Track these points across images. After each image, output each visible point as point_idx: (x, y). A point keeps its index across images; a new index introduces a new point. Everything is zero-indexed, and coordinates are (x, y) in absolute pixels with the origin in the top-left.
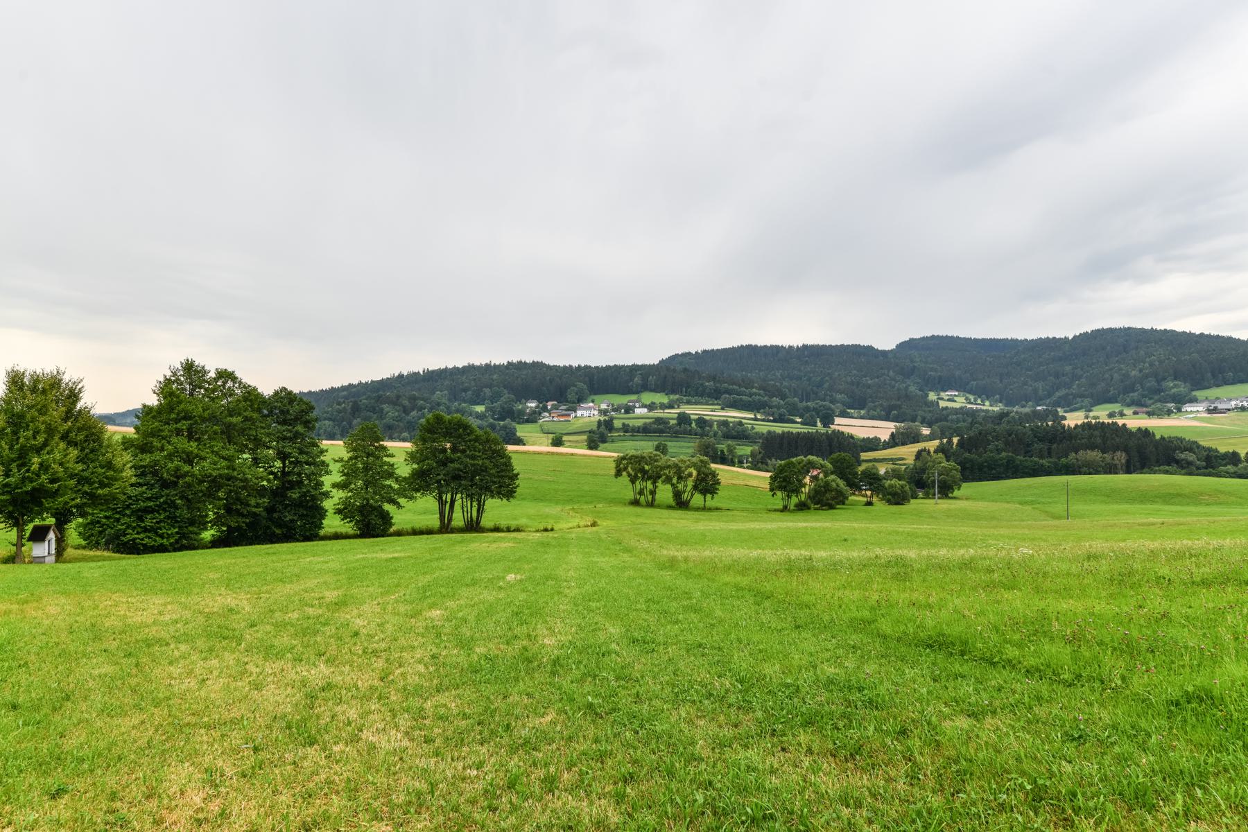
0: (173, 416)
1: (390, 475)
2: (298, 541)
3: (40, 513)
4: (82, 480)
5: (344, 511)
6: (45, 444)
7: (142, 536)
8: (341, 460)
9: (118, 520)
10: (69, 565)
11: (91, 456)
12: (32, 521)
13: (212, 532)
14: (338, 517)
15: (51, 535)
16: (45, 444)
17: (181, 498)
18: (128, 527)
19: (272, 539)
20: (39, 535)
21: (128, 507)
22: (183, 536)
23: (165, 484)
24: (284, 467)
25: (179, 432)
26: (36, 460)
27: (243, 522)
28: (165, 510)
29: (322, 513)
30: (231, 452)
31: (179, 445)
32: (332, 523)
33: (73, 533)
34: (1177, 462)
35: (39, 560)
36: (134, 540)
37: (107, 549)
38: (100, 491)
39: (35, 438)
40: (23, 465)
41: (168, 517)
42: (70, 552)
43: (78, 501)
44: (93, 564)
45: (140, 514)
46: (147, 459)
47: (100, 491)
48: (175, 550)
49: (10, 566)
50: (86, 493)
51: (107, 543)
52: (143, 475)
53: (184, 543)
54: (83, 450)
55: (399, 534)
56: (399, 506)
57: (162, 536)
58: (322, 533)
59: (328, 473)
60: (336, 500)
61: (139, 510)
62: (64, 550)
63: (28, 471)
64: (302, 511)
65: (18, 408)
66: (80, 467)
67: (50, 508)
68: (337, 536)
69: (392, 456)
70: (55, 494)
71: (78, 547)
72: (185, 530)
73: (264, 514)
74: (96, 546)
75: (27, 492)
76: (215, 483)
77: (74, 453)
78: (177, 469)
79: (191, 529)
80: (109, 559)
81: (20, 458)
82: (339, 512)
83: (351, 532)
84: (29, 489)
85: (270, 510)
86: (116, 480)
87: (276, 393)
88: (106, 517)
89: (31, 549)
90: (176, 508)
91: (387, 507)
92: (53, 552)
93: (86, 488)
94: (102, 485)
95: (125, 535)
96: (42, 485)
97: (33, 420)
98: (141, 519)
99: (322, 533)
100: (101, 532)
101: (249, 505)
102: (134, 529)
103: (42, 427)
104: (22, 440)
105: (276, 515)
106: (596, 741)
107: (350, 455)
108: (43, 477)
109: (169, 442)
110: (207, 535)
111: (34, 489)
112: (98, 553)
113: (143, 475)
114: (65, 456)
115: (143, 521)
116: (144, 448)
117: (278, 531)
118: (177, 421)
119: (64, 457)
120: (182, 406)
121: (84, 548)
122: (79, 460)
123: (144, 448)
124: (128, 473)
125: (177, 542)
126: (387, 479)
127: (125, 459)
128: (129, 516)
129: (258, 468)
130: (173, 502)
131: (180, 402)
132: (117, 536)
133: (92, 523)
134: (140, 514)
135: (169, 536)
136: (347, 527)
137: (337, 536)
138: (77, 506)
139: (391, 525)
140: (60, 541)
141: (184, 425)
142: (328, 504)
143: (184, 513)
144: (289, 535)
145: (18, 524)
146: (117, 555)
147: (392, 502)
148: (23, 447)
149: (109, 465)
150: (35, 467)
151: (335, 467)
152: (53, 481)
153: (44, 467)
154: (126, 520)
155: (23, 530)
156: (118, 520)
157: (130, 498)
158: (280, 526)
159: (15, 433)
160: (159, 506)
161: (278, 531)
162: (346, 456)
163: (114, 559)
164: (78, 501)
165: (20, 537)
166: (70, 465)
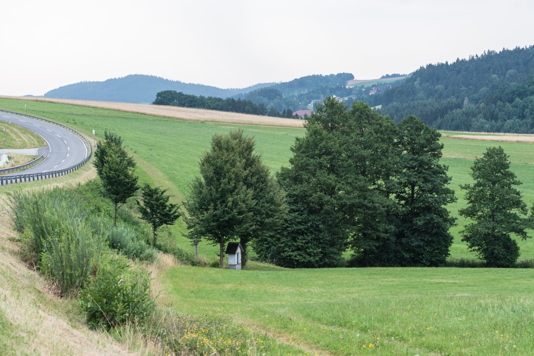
0: (317, 152)
1: (517, 203)
2: (424, 265)
3: (232, 235)
4: (257, 212)
5: (471, 238)
6: (235, 188)
7: (296, 253)
8: (467, 187)
9: (279, 239)
10: (251, 272)
11: (261, 194)
12: (228, 240)
13: (352, 252)
14: (465, 246)
15: (239, 250)
16: (235, 188)
17: (324, 223)
18: (286, 245)
19: (402, 263)
20: (231, 250)
21: (286, 228)
22: (325, 255)
23: (312, 211)
24: (413, 193)
25: (321, 166)
26: (230, 199)
27: (373, 245)
28: (311, 233)
29: (448, 240)
30: (361, 183)
31: (321, 178)
32: (459, 249)
33: (251, 252)
34: (422, 263)
35: (231, 267)
36: (290, 256)
37: (272, 262)
38: (267, 220)
39: (229, 183)
40: (223, 202)
41: (315, 239)
42: (249, 263)
43: (254, 227)
44: (264, 272)
45: (295, 235)
46: (298, 189)
47: (267, 220)
48: (320, 267)
49: (216, 269)
50: (258, 221)
51: (272, 258)
52: (295, 202)
53: (327, 261)
54: (255, 190)
55: (525, 265)
56: (524, 235)
57: (309, 254)
58: (448, 259)
59: (453, 200)
60: (461, 228)
61: (293, 232)
62: (246, 261)
63: (226, 206)
64: (427, 238)
65: (219, 162)
66: (254, 202)
67: (239, 232)
68: (463, 264)
69: (519, 183)
70: (240, 222)
71: (253, 259)
72: (327, 251)
73: (393, 239)
74: (264, 259)
75: (226, 221)
76: (351, 209)
77: (251, 192)
78: (320, 198)
79: (332, 250)
80: (273, 269)
81: (221, 197)
82: (466, 239)
83: (478, 261)
84: (227, 218)
85: (400, 235)
86: (276, 211)
87: (462, 60)
88: (271, 236)
89: (227, 259)
90: (320, 231)
91: (513, 236)
92: (240, 262)
93: (258, 218)
94: (268, 216)
95: (284, 252)
96: (233, 216)
97: (228, 171)
98: (294, 239)
99: (448, 259)
100: (268, 248)
101: (378, 231)
102: (290, 247)
103: (233, 176)
104: (222, 185)
105: (404, 240)
106: (330, 299)
107: (476, 182)
108: (235, 211)
109: (314, 175)
110: (348, 254)
111: (229, 219)
112: (267, 265)
113: (295, 202)
114: (246, 195)
115: (296, 241)
116: (297, 180)
117: (407, 256)
118: (320, 156)
119: (245, 195)
120: (324, 143)
121: (257, 260)
122: (255, 197)
123: (297, 180)
124: (284, 207)
125: (321, 259)
126: (511, 207)
127: (281, 195)
128: (286, 237)
129: (389, 195)
130: (317, 226)
131: (322, 140)
132: (280, 251)
133: (262, 241)
134: (295, 235)
135: (315, 255)
136: (474, 256)
137: (463, 264)
138: (254, 231)
139: (517, 255)
140: (244, 254)
141: (325, 160)
142: (452, 231)
143: (326, 236)
144: (416, 261)
145: (220, 241)
146: (279, 267)
147: (521, 232)
148: (223, 189)
149: (271, 201)
150: (230, 204)
151: (461, 195)
152: (240, 213)
153: (235, 204)
154: (283, 239)
155: (224, 246)
156: (279, 239)
157: (286, 221)
158: (408, 251)
159: (218, 180)
160: (307, 229)
161: (407, 256)
162: (472, 182)
163: (276, 270)
164: (254, 227)
165: (222, 250)
166: (249, 202)
